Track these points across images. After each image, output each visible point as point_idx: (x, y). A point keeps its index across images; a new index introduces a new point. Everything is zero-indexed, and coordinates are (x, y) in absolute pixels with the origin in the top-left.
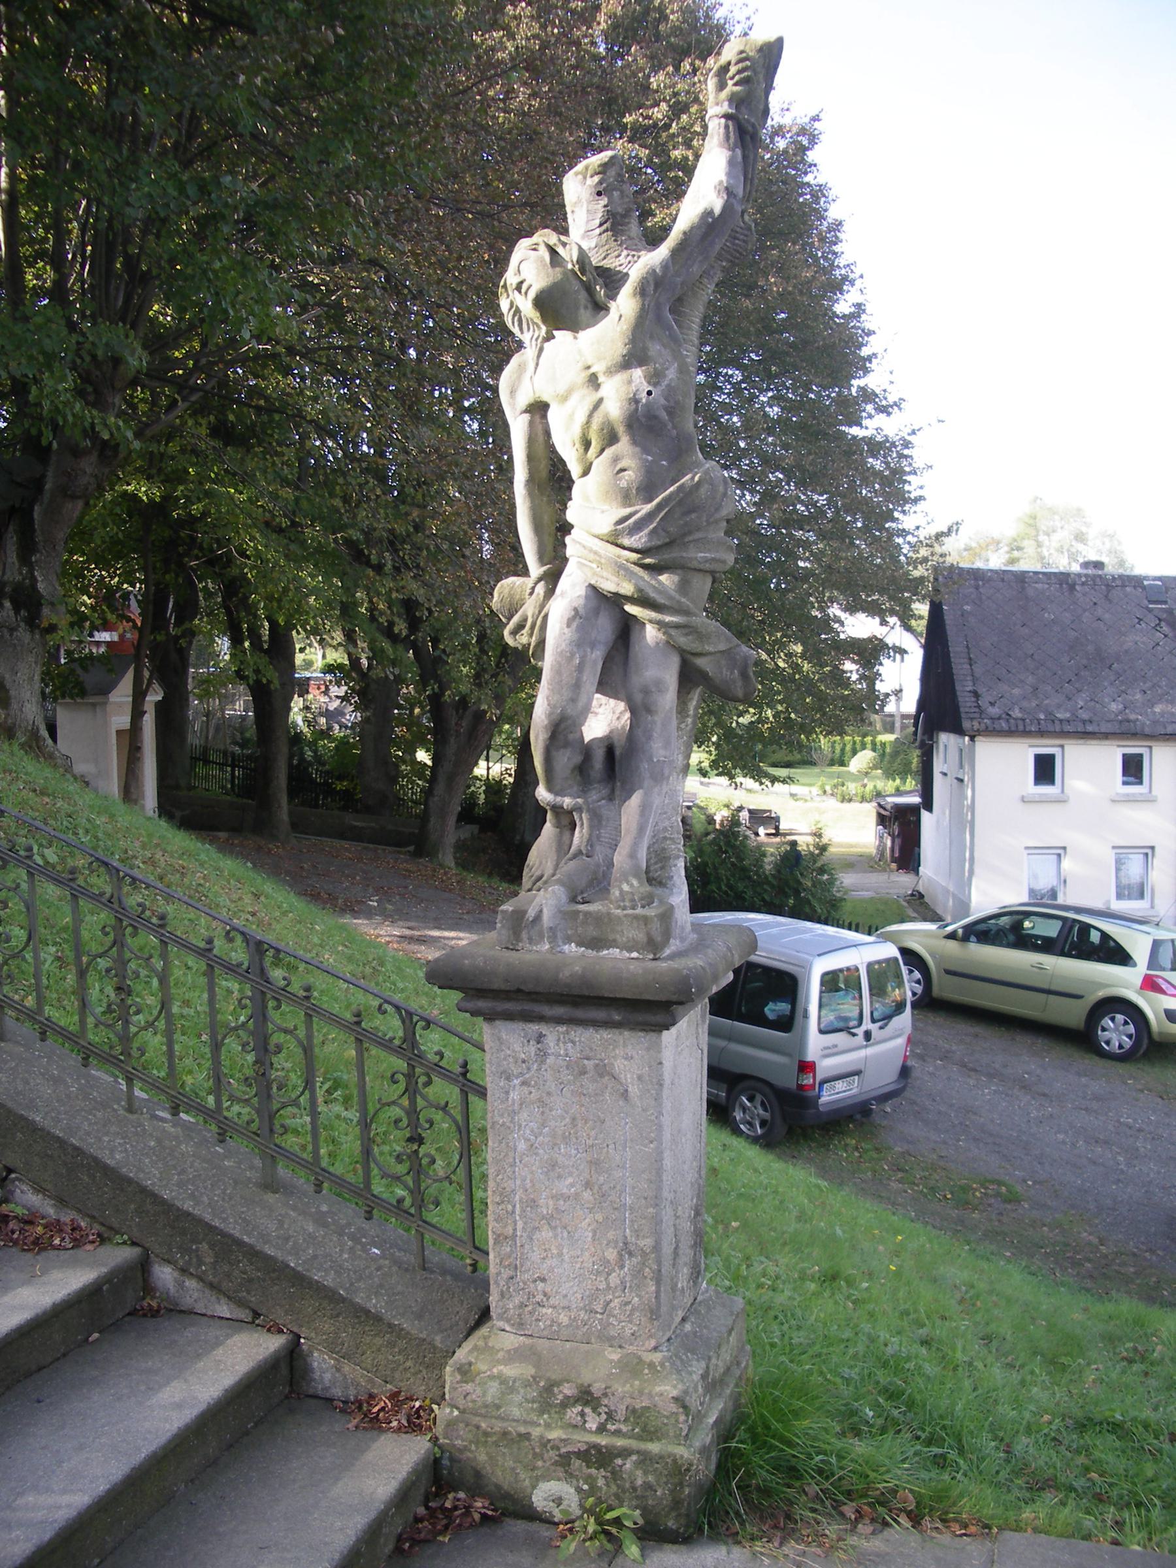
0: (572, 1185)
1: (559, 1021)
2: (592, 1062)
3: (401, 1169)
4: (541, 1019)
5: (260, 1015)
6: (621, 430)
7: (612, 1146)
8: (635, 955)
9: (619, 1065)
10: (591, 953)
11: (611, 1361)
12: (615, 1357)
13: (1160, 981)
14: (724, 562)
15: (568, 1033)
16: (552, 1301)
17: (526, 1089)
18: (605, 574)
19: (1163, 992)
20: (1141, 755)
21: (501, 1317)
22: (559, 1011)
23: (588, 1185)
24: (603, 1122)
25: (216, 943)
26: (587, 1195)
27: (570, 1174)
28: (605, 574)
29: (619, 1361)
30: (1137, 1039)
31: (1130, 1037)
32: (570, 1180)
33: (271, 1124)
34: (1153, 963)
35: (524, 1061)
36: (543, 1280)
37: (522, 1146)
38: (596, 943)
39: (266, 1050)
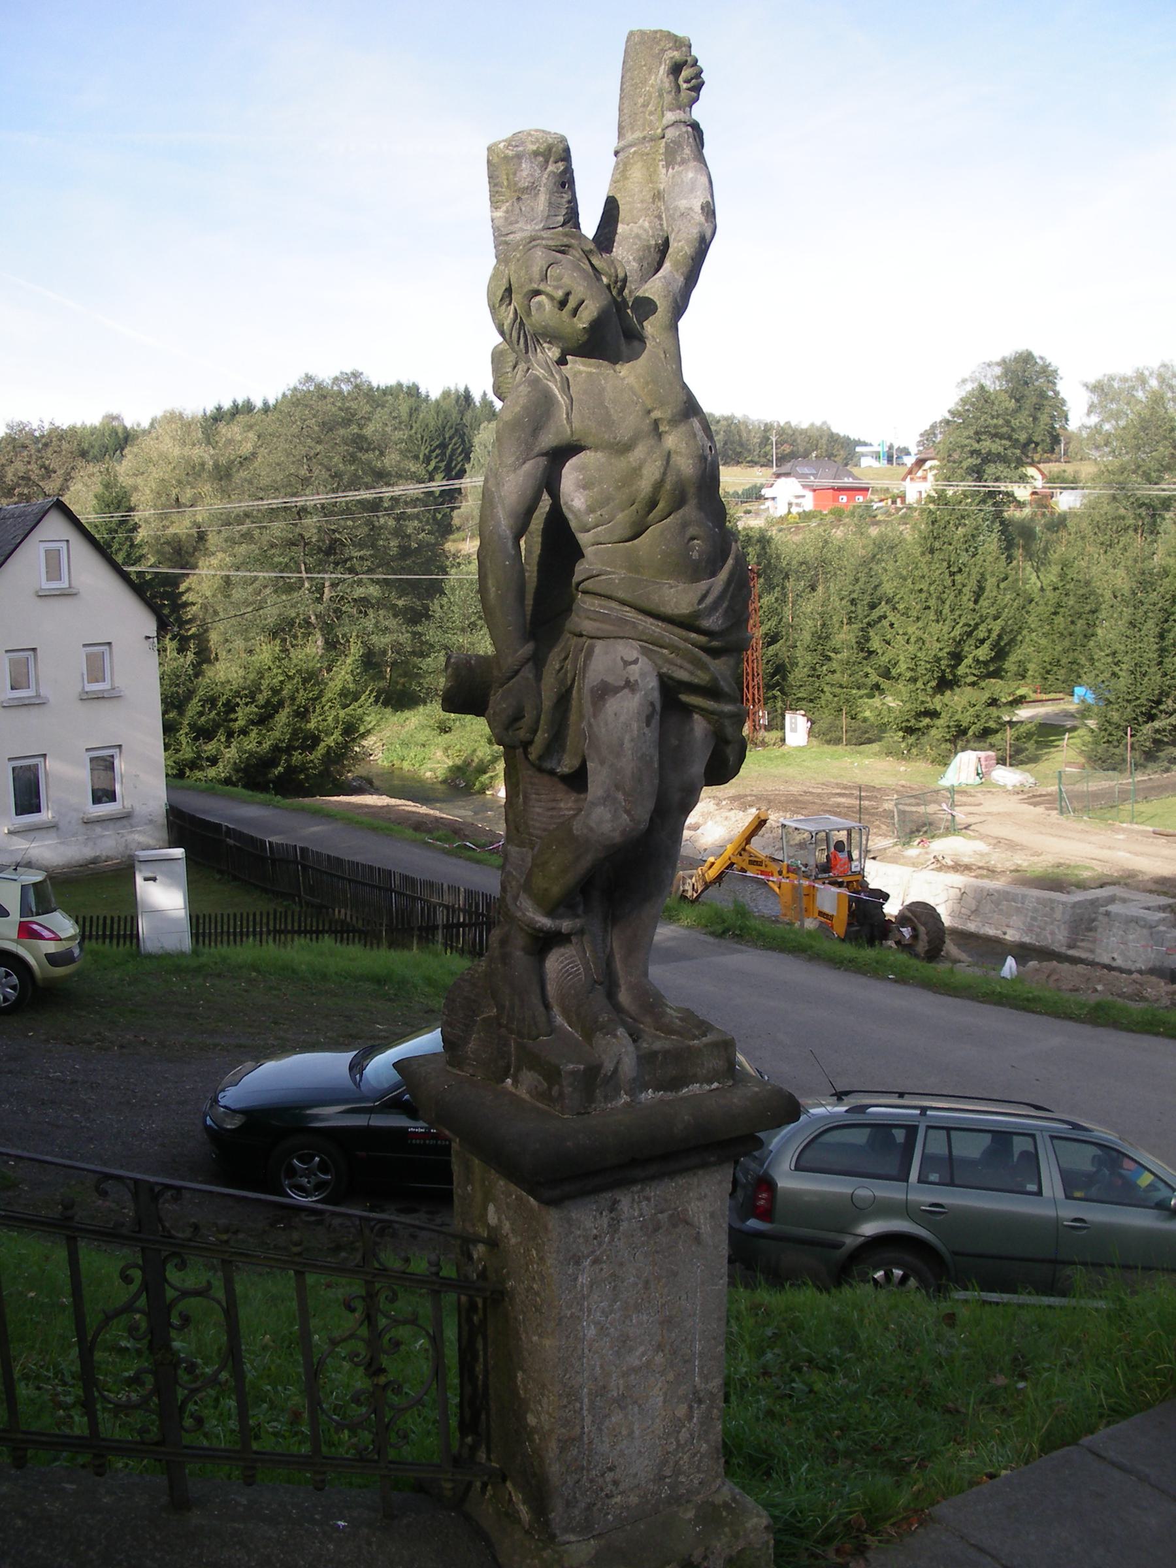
0: (643, 1354)
2: (666, 1215)
6: (691, 491)
7: (684, 1297)
8: (715, 1085)
10: (670, 1095)
11: (690, 1520)
12: (690, 1514)
13: (35, 927)
16: (621, 1488)
17: (597, 1267)
18: (679, 661)
19: (42, 938)
21: (566, 1530)
23: (660, 1347)
24: (675, 1274)
26: (659, 1359)
27: (641, 1344)
28: (679, 661)
29: (696, 1516)
30: (22, 989)
31: (13, 988)
32: (641, 1349)
34: (25, 910)
35: (595, 1237)
36: (611, 1469)
37: (592, 1332)
38: (674, 1084)
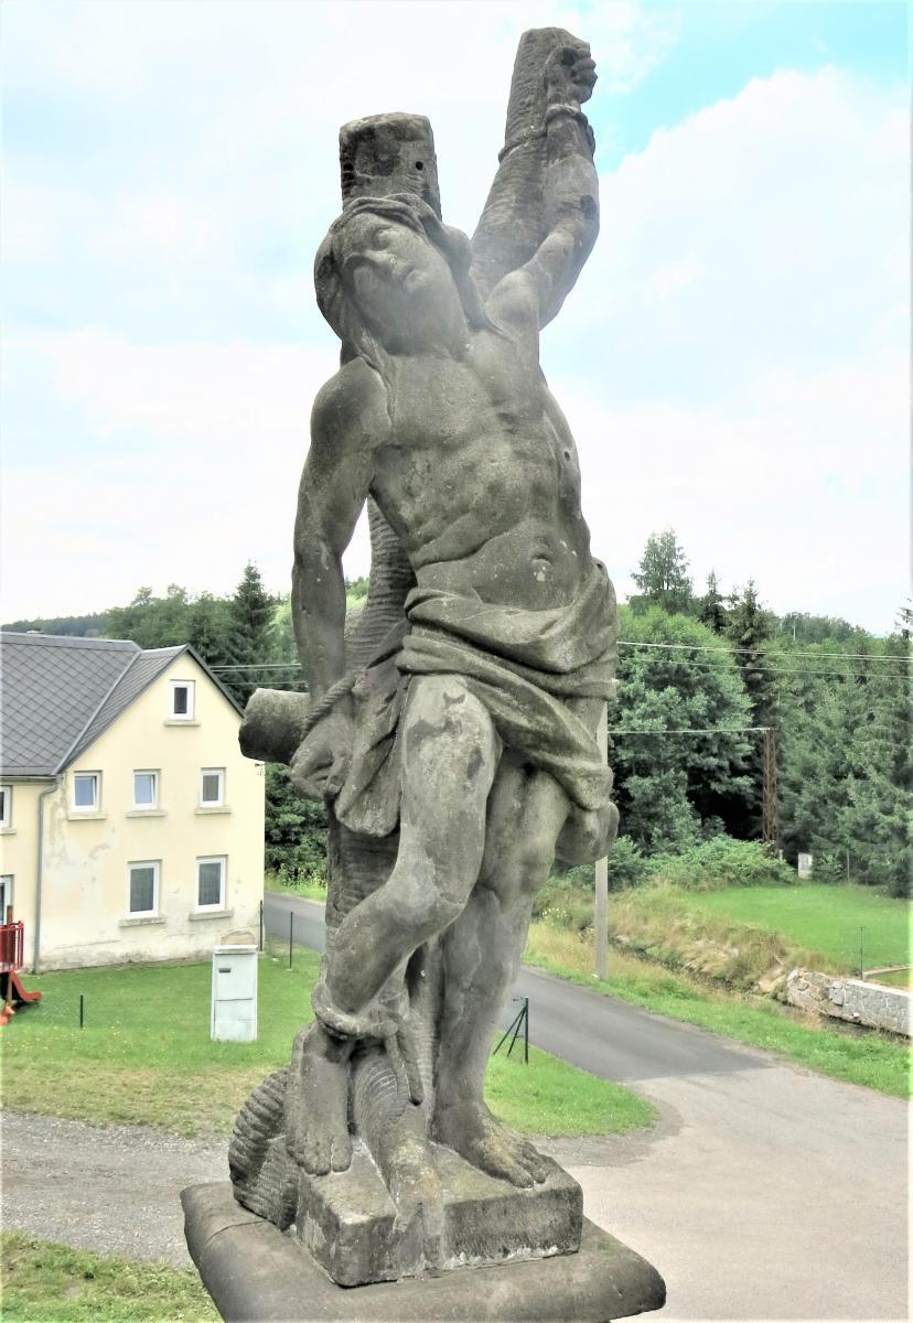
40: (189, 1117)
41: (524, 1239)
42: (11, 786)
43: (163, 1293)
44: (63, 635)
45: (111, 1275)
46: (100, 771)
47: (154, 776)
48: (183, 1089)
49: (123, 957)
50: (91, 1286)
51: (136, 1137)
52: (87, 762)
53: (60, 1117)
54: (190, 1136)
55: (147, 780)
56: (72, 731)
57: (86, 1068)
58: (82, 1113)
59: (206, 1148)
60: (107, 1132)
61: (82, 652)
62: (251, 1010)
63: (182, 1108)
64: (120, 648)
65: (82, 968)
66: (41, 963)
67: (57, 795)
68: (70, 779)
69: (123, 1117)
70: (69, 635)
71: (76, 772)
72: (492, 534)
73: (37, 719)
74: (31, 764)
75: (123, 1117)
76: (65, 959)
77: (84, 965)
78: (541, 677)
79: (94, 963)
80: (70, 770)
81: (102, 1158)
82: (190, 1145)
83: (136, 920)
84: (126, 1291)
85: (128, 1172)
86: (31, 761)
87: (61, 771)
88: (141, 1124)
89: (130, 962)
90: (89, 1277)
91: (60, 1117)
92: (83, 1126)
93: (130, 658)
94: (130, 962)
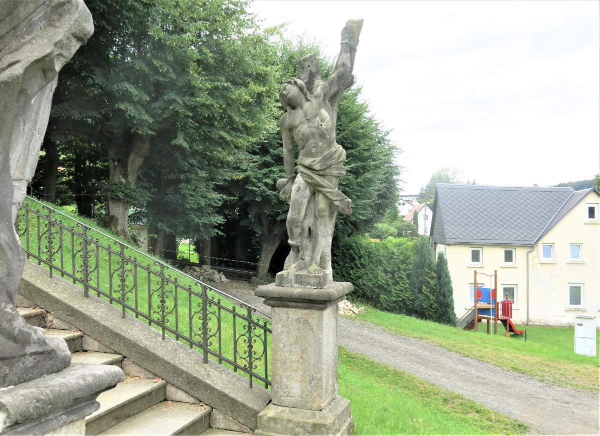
1: (293, 307)
3: (200, 332)
4: (287, 307)
5: (204, 309)
9: (310, 320)
14: (342, 174)
15: (296, 311)
20: (479, 251)
22: (293, 304)
25: (112, 246)
33: (207, 342)
39: (206, 319)
40: (544, 375)
41: (309, 284)
42: (515, 248)
43: (502, 424)
44: (581, 189)
45: (485, 414)
46: (554, 243)
47: (579, 246)
48: (547, 365)
49: (567, 324)
50: (478, 415)
51: (519, 377)
52: (547, 239)
53: (492, 364)
54: (541, 381)
55: (576, 247)
56: (544, 224)
57: (511, 352)
58: (501, 365)
59: (547, 387)
60: (508, 373)
61: (534, 193)
62: (593, 343)
63: (543, 372)
64: (564, 190)
65: (548, 326)
66: (530, 321)
67: (535, 253)
68: (540, 246)
69: (516, 369)
70: (584, 189)
71: (543, 243)
72: (306, 143)
73: (526, 221)
74: (523, 240)
75: (516, 369)
76: (540, 321)
77: (549, 325)
78: (314, 172)
79: (553, 324)
80: (540, 242)
81: (503, 381)
82: (540, 384)
83: (572, 308)
84: (490, 420)
85: (511, 387)
86: (523, 238)
87: (535, 243)
88: (523, 373)
89: (570, 326)
90: (477, 412)
91: (492, 364)
92: (500, 369)
93: (569, 195)
94: (570, 326)
